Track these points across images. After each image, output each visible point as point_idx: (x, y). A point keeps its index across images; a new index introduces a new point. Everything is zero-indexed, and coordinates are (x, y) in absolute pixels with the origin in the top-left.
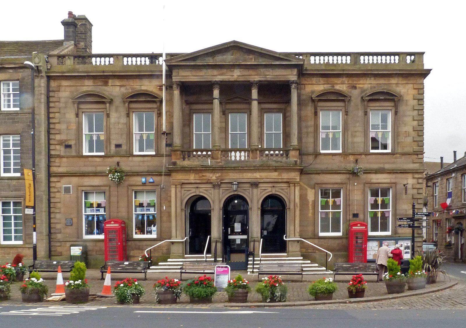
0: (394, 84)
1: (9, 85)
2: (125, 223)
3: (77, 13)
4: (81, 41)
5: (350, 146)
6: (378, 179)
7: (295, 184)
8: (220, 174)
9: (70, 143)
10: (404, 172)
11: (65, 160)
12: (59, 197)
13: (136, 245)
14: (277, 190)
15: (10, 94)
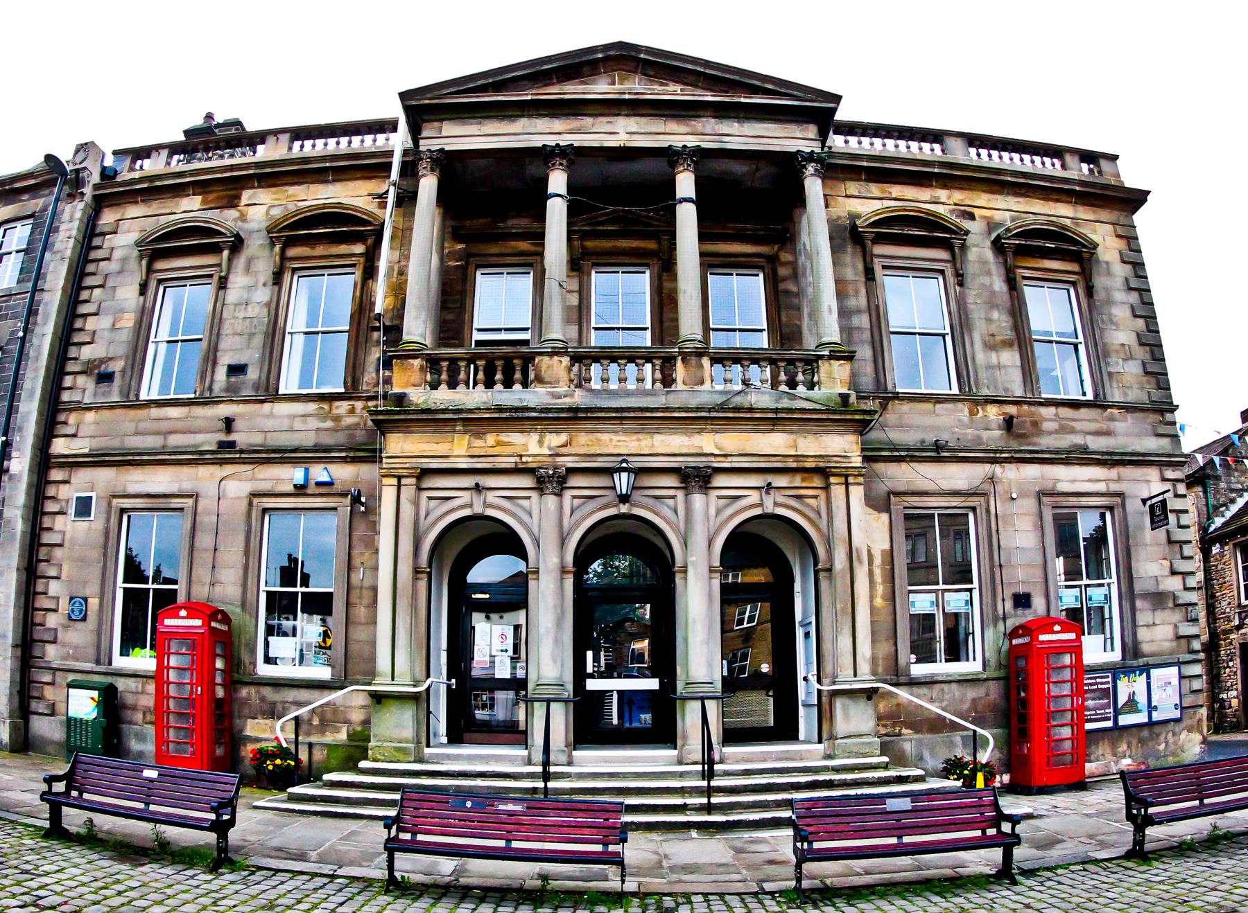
2: (226, 619)
5: (983, 375)
6: (1074, 481)
7: (846, 477)
8: (563, 438)
11: (90, 416)
13: (263, 699)
14: (780, 500)
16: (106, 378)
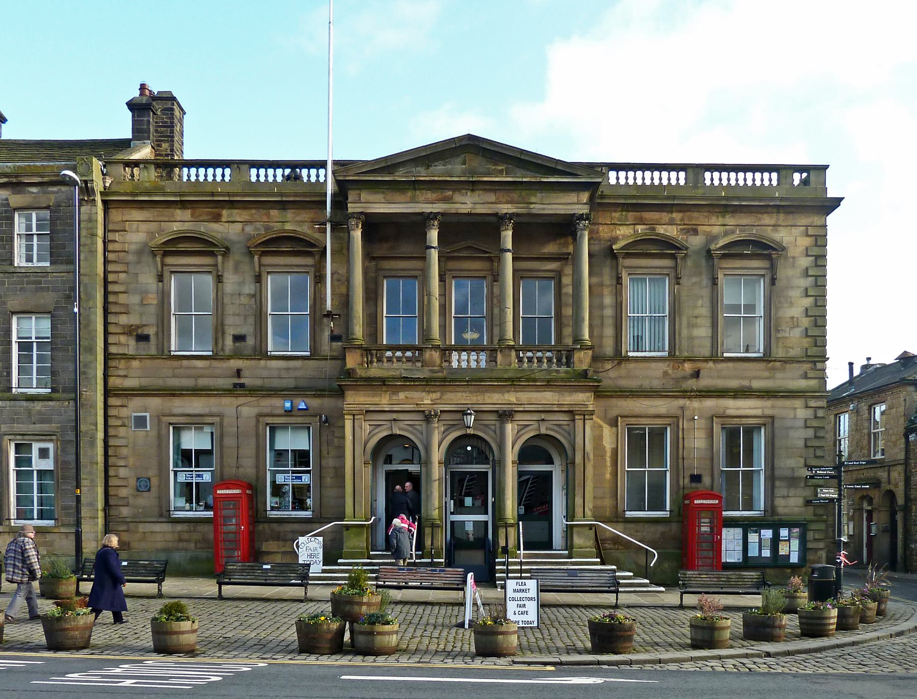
0: (769, 226)
1: (29, 219)
3: (156, 87)
4: (163, 141)
5: (685, 344)
6: (738, 409)
7: (584, 415)
8: (439, 394)
9: (146, 331)
10: (791, 394)
11: (135, 364)
12: (125, 435)
15: (33, 234)
16: (143, 338)
